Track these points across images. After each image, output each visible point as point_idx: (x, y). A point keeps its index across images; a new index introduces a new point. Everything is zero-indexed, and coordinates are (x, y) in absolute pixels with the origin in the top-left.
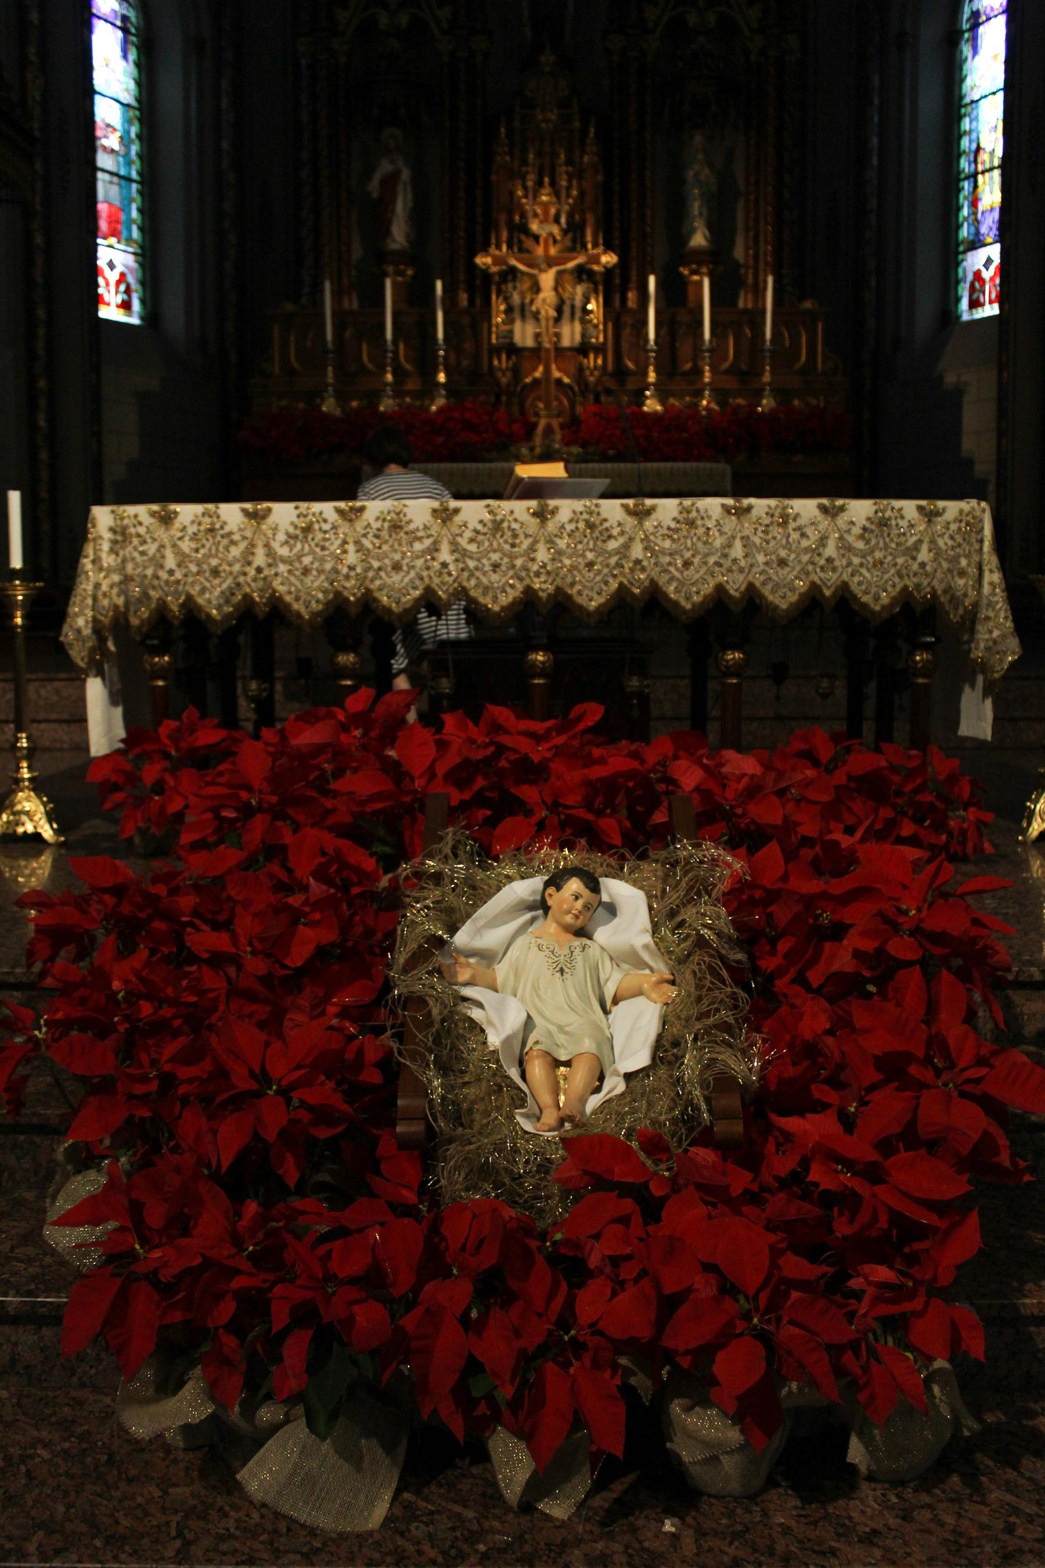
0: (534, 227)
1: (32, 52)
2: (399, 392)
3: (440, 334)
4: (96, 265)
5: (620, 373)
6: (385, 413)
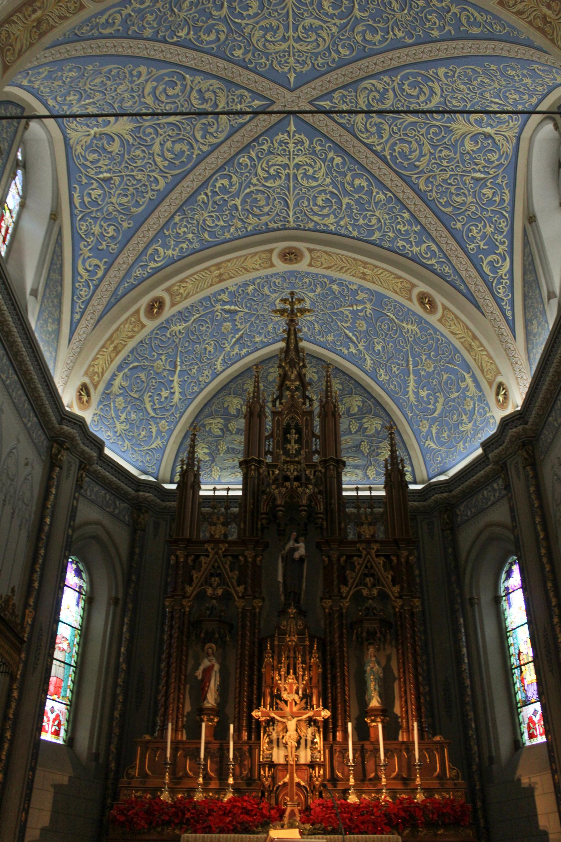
0: (285, 695)
1: (31, 601)
2: (206, 790)
3: (231, 756)
4: (44, 710)
5: (334, 780)
6: (197, 801)
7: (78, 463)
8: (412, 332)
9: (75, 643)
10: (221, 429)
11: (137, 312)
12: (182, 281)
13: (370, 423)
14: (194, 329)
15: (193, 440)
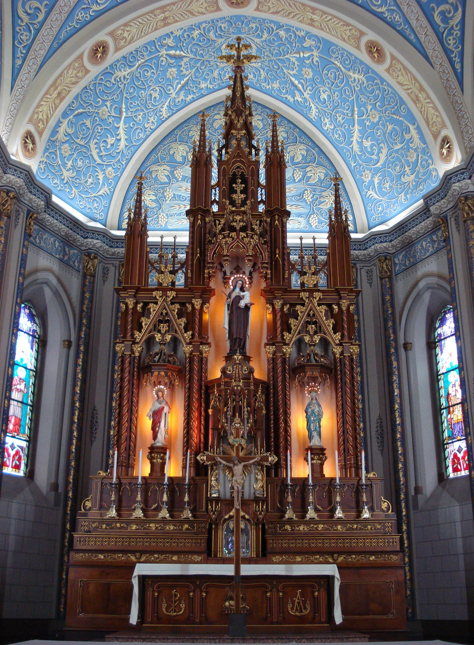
7: (25, 212)
8: (359, 81)
9: (31, 384)
10: (168, 176)
11: (81, 57)
12: (126, 25)
13: (313, 172)
14: (139, 75)
15: (140, 189)
